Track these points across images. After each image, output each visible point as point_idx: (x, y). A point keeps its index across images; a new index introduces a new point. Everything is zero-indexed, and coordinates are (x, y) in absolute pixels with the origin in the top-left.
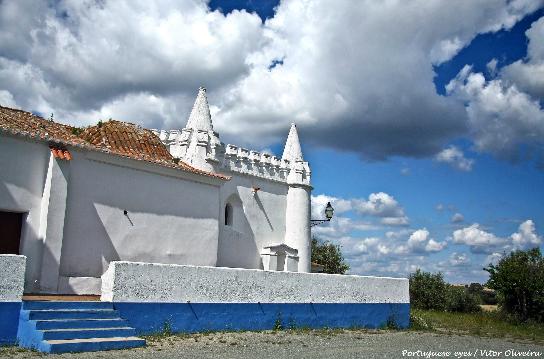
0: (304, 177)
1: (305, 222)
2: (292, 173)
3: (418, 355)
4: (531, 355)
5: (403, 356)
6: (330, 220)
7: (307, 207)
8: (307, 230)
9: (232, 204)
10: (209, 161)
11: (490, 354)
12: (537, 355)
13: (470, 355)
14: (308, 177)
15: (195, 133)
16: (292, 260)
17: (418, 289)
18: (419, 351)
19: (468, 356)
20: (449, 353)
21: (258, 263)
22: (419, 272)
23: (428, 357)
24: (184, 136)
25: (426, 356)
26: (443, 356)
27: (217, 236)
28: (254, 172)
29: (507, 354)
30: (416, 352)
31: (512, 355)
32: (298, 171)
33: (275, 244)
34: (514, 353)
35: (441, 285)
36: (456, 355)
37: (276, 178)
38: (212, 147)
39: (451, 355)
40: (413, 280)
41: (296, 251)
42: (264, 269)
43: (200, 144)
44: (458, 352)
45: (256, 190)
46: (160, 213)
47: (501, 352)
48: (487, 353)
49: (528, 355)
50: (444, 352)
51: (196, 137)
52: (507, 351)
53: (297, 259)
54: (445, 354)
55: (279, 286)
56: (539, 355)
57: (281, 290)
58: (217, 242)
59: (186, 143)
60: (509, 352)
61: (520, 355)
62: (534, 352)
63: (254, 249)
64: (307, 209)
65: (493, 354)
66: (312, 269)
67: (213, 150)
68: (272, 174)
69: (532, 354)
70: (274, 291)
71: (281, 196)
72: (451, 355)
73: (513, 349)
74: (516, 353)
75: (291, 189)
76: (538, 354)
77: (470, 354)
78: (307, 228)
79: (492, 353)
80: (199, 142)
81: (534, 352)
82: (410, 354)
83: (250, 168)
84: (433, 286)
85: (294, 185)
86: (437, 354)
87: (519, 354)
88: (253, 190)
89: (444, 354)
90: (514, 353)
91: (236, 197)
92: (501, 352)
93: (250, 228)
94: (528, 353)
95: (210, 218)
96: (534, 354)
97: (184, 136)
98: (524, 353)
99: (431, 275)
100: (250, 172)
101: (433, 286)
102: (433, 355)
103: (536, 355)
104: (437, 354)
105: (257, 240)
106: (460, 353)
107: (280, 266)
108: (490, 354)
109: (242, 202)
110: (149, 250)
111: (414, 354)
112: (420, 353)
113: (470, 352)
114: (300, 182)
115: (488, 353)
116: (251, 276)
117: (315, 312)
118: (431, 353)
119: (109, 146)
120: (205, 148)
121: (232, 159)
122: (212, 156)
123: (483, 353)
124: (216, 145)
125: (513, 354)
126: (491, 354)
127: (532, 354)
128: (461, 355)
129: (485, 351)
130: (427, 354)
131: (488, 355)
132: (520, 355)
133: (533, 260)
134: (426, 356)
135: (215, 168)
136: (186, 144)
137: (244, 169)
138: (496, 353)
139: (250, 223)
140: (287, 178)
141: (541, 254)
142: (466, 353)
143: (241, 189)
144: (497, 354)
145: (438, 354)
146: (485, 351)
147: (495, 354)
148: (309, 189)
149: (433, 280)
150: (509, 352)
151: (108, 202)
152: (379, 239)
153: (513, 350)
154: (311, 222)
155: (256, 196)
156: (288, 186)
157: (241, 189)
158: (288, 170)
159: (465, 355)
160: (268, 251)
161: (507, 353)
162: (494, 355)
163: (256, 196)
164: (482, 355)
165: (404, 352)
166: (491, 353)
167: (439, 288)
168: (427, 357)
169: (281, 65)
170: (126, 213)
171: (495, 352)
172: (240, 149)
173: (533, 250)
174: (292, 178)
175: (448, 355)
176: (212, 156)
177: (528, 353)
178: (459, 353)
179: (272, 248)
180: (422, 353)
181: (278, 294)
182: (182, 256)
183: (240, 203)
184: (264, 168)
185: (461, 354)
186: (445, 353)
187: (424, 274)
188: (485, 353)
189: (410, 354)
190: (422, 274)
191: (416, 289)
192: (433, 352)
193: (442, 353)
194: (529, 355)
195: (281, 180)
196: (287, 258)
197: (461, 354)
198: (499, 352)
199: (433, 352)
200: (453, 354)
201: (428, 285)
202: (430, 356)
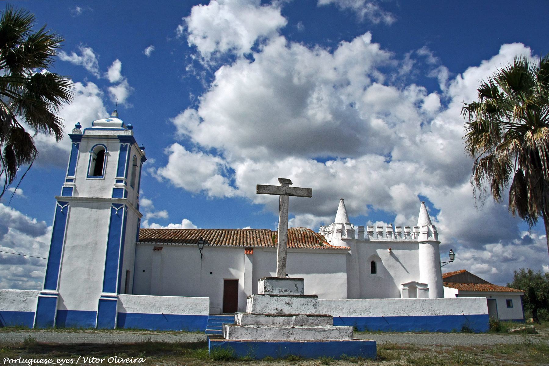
2: (421, 234)
3: (20, 363)
4: (135, 362)
5: (5, 363)
6: (453, 261)
9: (376, 261)
10: (343, 240)
13: (73, 362)
16: (423, 291)
18: (20, 359)
19: (71, 363)
20: (51, 360)
21: (398, 294)
23: (30, 364)
25: (28, 363)
27: (346, 282)
30: (18, 360)
31: (116, 362)
34: (117, 359)
38: (346, 231)
39: (54, 362)
42: (444, 297)
47: (104, 359)
50: (46, 359)
52: (110, 358)
54: (47, 362)
55: (355, 308)
57: (357, 310)
58: (347, 285)
60: (112, 359)
61: (123, 362)
62: (138, 359)
63: (394, 286)
64: (433, 256)
67: (346, 233)
69: (135, 360)
70: (351, 310)
71: (413, 251)
72: (54, 362)
74: (119, 360)
75: (420, 245)
77: (72, 361)
78: (434, 269)
79: (94, 360)
81: (138, 359)
82: (11, 361)
85: (421, 242)
86: (39, 361)
91: (376, 256)
92: (104, 359)
93: (389, 273)
94: (131, 360)
95: (341, 272)
102: (35, 363)
104: (39, 361)
105: (396, 281)
106: (62, 360)
109: (381, 259)
111: (15, 361)
112: (21, 361)
113: (72, 359)
114: (426, 240)
116: (333, 302)
117: (387, 322)
120: (341, 233)
123: (86, 360)
124: (347, 230)
125: (116, 361)
126: (94, 361)
127: (135, 360)
128: (63, 362)
129: (88, 358)
130: (28, 362)
132: (123, 362)
134: (28, 363)
138: (99, 360)
139: (389, 270)
140: (417, 238)
143: (380, 252)
144: (100, 361)
145: (40, 361)
146: (88, 358)
150: (112, 359)
152: (543, 266)
153: (116, 357)
155: (392, 254)
156: (418, 243)
157: (380, 252)
159: (67, 363)
160: (402, 287)
162: (96, 362)
163: (392, 254)
164: (85, 362)
165: (5, 359)
166: (93, 360)
171: (98, 359)
176: (345, 237)
177: (131, 360)
178: (61, 360)
180: (23, 360)
181: (354, 312)
183: (380, 260)
185: (19, 361)
186: (47, 360)
188: (88, 361)
189: (11, 361)
192: (35, 360)
197: (19, 361)
198: (102, 359)
199: (35, 360)
200: (55, 361)
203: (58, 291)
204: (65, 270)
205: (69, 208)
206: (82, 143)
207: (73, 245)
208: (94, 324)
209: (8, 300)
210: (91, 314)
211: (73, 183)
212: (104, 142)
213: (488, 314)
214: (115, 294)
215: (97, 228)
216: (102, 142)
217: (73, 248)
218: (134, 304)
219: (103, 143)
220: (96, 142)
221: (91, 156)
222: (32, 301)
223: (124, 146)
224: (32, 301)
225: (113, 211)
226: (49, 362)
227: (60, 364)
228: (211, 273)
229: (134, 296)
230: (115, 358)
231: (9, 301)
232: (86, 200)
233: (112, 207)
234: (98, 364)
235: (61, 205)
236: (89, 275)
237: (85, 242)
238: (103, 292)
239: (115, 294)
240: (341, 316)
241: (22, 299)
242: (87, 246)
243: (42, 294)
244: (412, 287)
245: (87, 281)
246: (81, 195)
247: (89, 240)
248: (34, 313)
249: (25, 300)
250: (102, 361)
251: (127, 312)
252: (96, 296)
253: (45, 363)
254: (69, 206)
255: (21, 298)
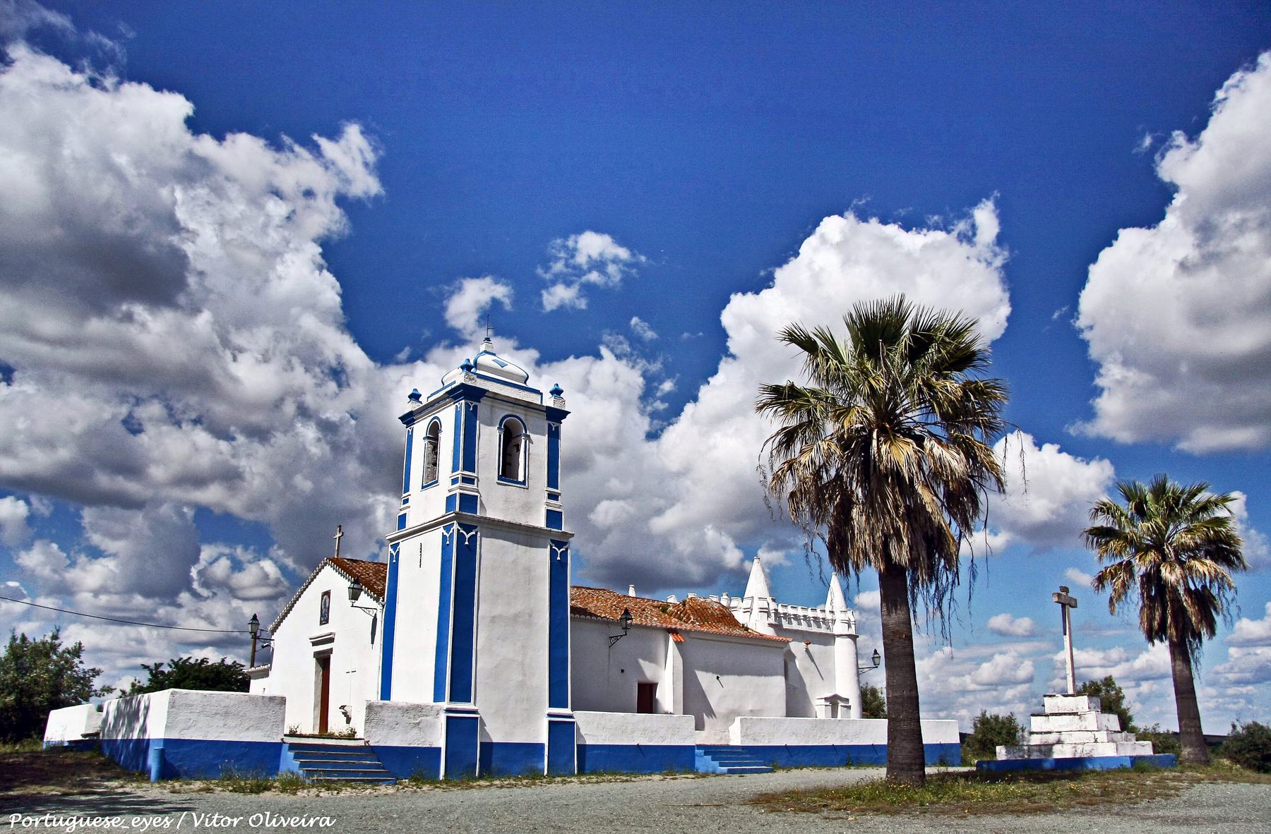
0: (849, 626)
1: (854, 671)
4: (311, 826)
7: (855, 656)
8: (856, 678)
10: (770, 625)
11: (214, 821)
12: (270, 825)
13: (168, 824)
14: (853, 626)
15: (756, 600)
16: (845, 709)
17: (985, 736)
19: (105, 826)
22: (985, 715)
24: (747, 603)
26: (164, 826)
28: (804, 627)
29: (254, 822)
32: (843, 621)
33: (829, 695)
35: (1013, 729)
36: (136, 824)
37: (823, 630)
40: (979, 725)
41: (847, 700)
43: (762, 610)
44: (101, 819)
45: (807, 644)
46: (741, 674)
47: (242, 818)
48: (207, 820)
49: (303, 825)
51: (758, 604)
52: (255, 816)
53: (849, 707)
54: (108, 823)
56: (329, 825)
58: (785, 697)
59: (749, 610)
60: (258, 818)
61: (285, 825)
62: (318, 818)
65: (222, 821)
66: (864, 716)
68: (819, 627)
69: (312, 822)
71: (829, 647)
73: (267, 811)
74: (274, 820)
75: (837, 639)
76: (327, 822)
79: (218, 821)
80: (761, 608)
81: (318, 818)
83: (800, 624)
84: (1004, 731)
87: (282, 824)
88: (805, 645)
89: (167, 822)
90: (270, 821)
96: (316, 823)
97: (747, 603)
98: (157, 820)
99: (1000, 716)
100: (800, 628)
101: (1004, 731)
103: (321, 825)
106: (144, 820)
107: (834, 714)
108: (214, 821)
110: (736, 707)
115: (211, 820)
118: (77, 821)
119: (697, 623)
121: (785, 618)
122: (772, 620)
125: (269, 824)
126: (217, 823)
127: (312, 822)
128: (147, 825)
129: (203, 815)
131: (211, 824)
132: (285, 825)
133: (1108, 691)
135: (776, 632)
136: (749, 611)
137: (795, 626)
141: (1114, 684)
142: (296, 819)
144: (232, 822)
146: (203, 815)
147: (225, 823)
148: (853, 638)
149: (1003, 723)
150: (258, 818)
151: (706, 669)
153: (268, 813)
154: (859, 672)
155: (807, 650)
156: (834, 636)
158: (834, 621)
159: (156, 826)
161: (254, 819)
162: (223, 825)
163: (807, 650)
164: (196, 824)
166: (215, 821)
167: (1012, 734)
168: (67, 830)
169: (6, 387)
170: (718, 678)
171: (227, 818)
172: (810, 609)
173: (1106, 679)
174: (839, 628)
175: (116, 824)
176: (772, 620)
177: (303, 820)
178: (141, 820)
179: (826, 699)
182: (759, 710)
184: (812, 622)
187: (991, 716)
188: (203, 822)
190: (989, 717)
191: (982, 736)
193: (162, 821)
194: (305, 824)
195: (828, 632)
196: (839, 707)
197: (284, 822)
198: (236, 819)
201: (997, 730)
202: (74, 826)
203: (475, 704)
204: (482, 664)
205: (478, 539)
206: (483, 407)
207: (493, 615)
208: (540, 767)
209: (386, 723)
210: (536, 748)
211: (475, 486)
212: (520, 413)
213: (885, 742)
214: (567, 711)
215: (529, 584)
216: (517, 412)
217: (493, 620)
218: (598, 727)
219: (518, 415)
220: (507, 410)
221: (500, 436)
222: (432, 726)
223: (553, 429)
224: (431, 726)
225: (553, 553)
226: (113, 825)
227: (138, 829)
228: (622, 671)
229: (597, 715)
230: (265, 815)
231: (387, 725)
232: (508, 527)
233: (551, 547)
234: (276, 830)
235: (463, 530)
236: (524, 675)
237: (512, 611)
238: (550, 706)
239: (567, 711)
240: (642, 743)
241: (412, 721)
242: (516, 617)
243: (448, 711)
244: (834, 701)
245: (522, 685)
246: (491, 514)
247: (519, 607)
248: (439, 749)
249: (419, 724)
250: (236, 821)
251: (587, 743)
252: (539, 714)
253: (105, 826)
254: (479, 534)
255: (410, 718)
